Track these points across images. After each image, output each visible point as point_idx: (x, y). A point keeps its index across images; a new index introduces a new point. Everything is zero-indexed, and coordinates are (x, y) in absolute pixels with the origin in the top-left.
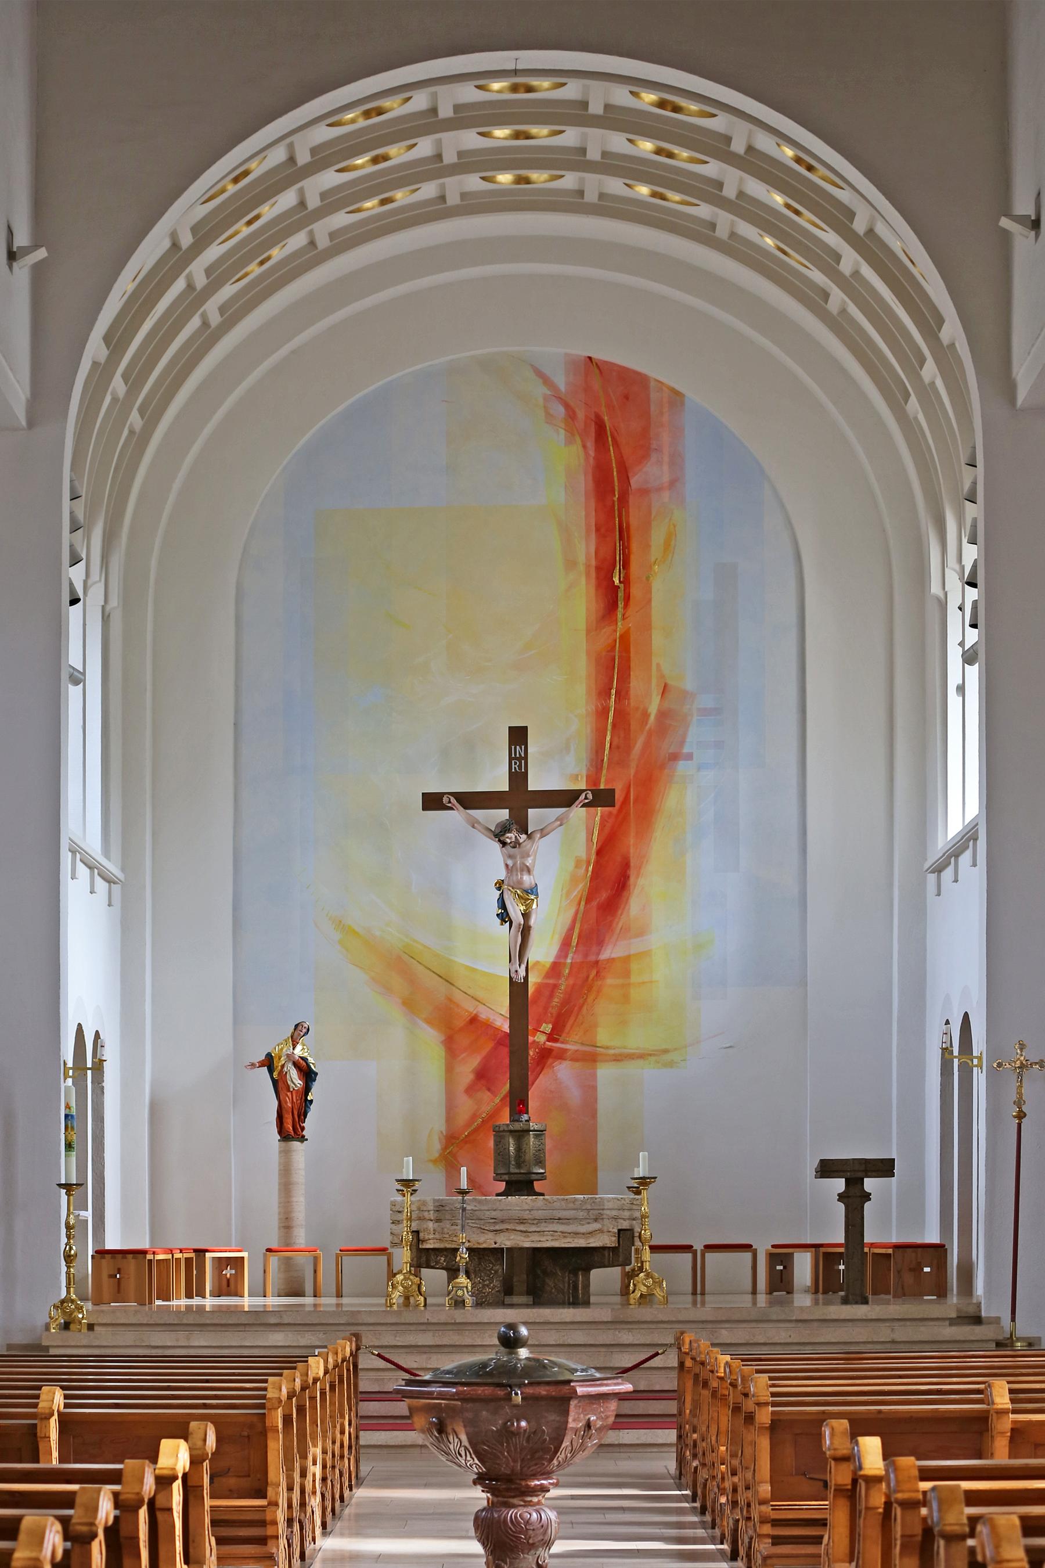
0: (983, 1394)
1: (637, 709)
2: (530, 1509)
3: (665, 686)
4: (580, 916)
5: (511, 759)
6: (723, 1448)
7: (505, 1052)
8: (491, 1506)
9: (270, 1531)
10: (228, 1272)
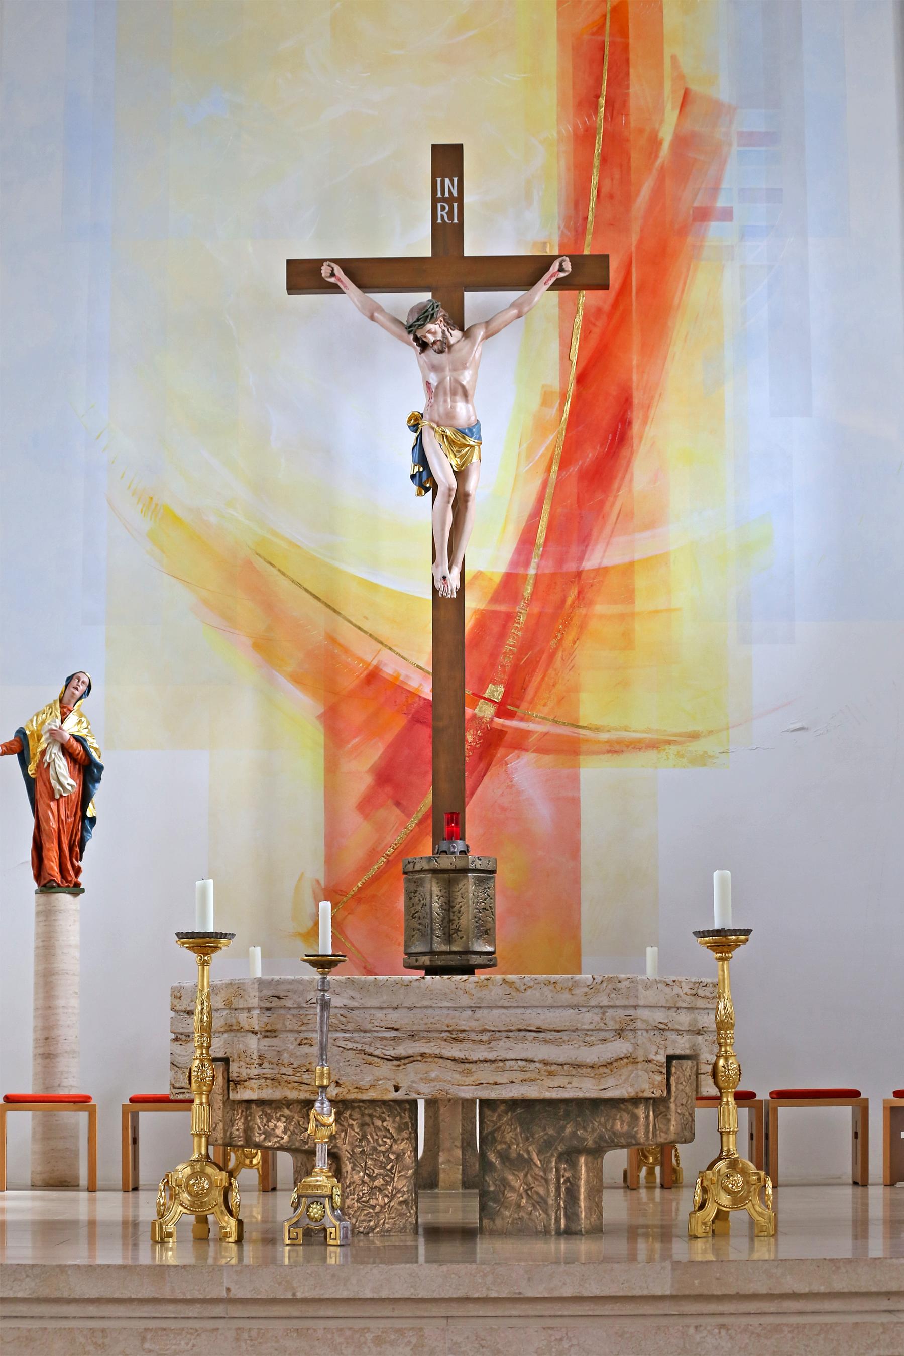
1: (641, 131)
3: (686, 93)
4: (550, 490)
7: (424, 734)
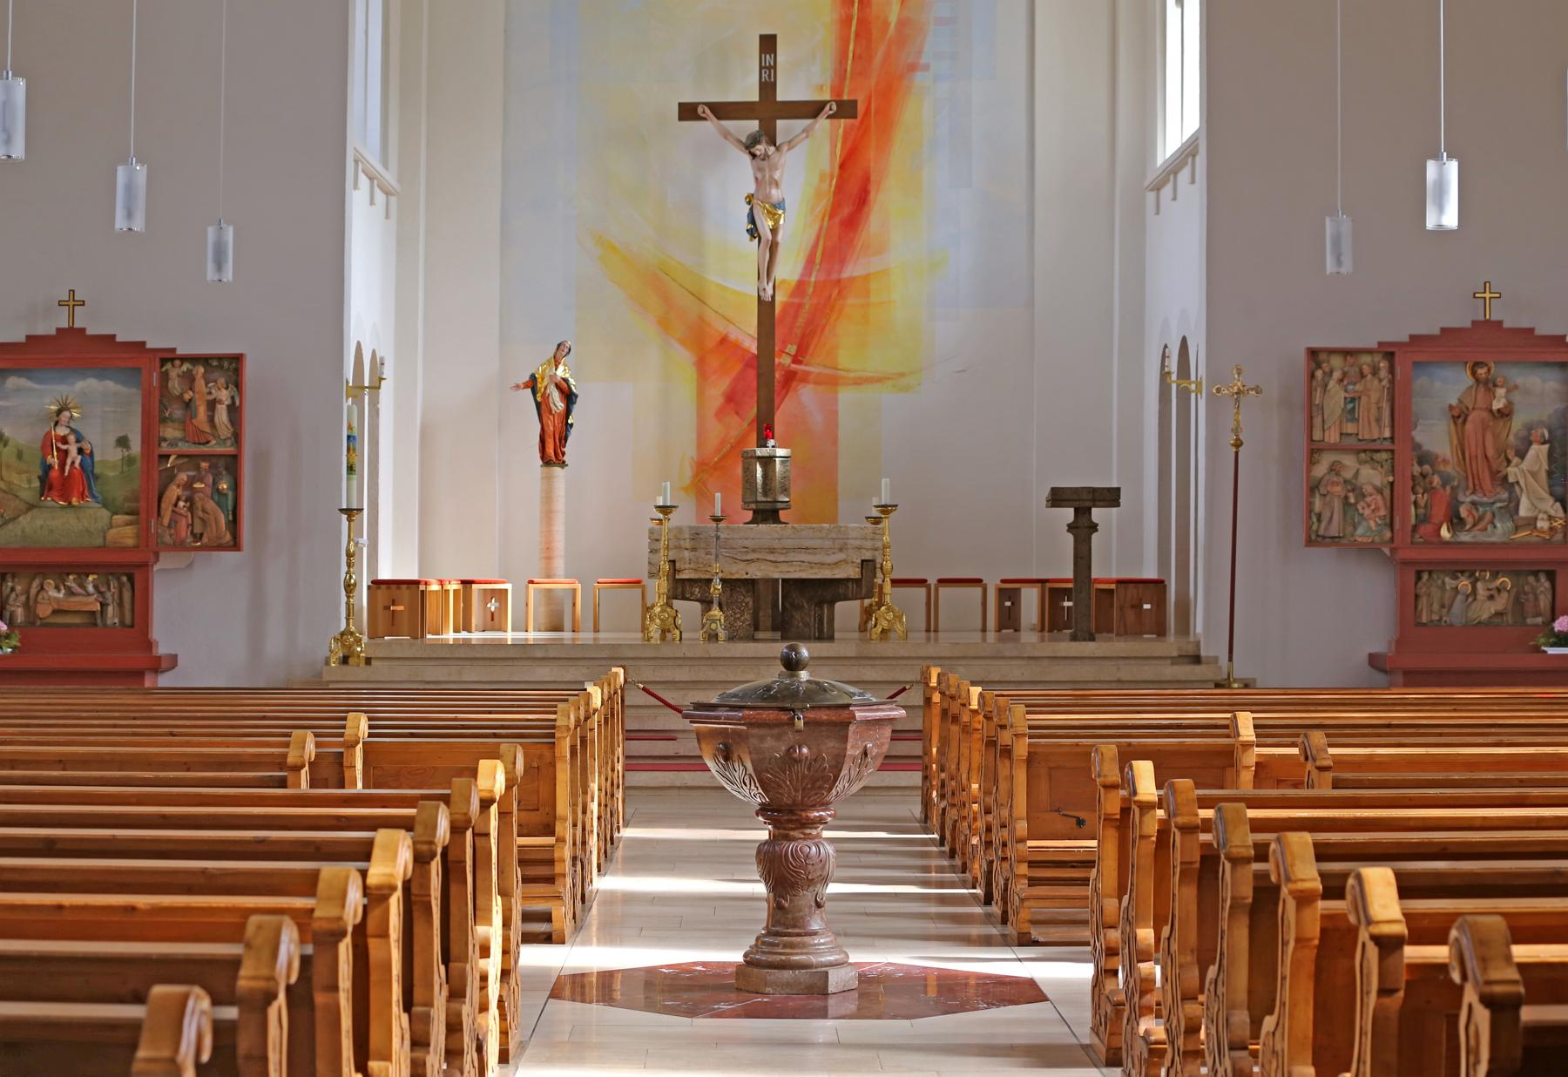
0: (1231, 728)
2: (809, 842)
5: (761, 68)
6: (975, 786)
7: (752, 373)
8: (774, 839)
9: (558, 869)
10: (493, 606)
